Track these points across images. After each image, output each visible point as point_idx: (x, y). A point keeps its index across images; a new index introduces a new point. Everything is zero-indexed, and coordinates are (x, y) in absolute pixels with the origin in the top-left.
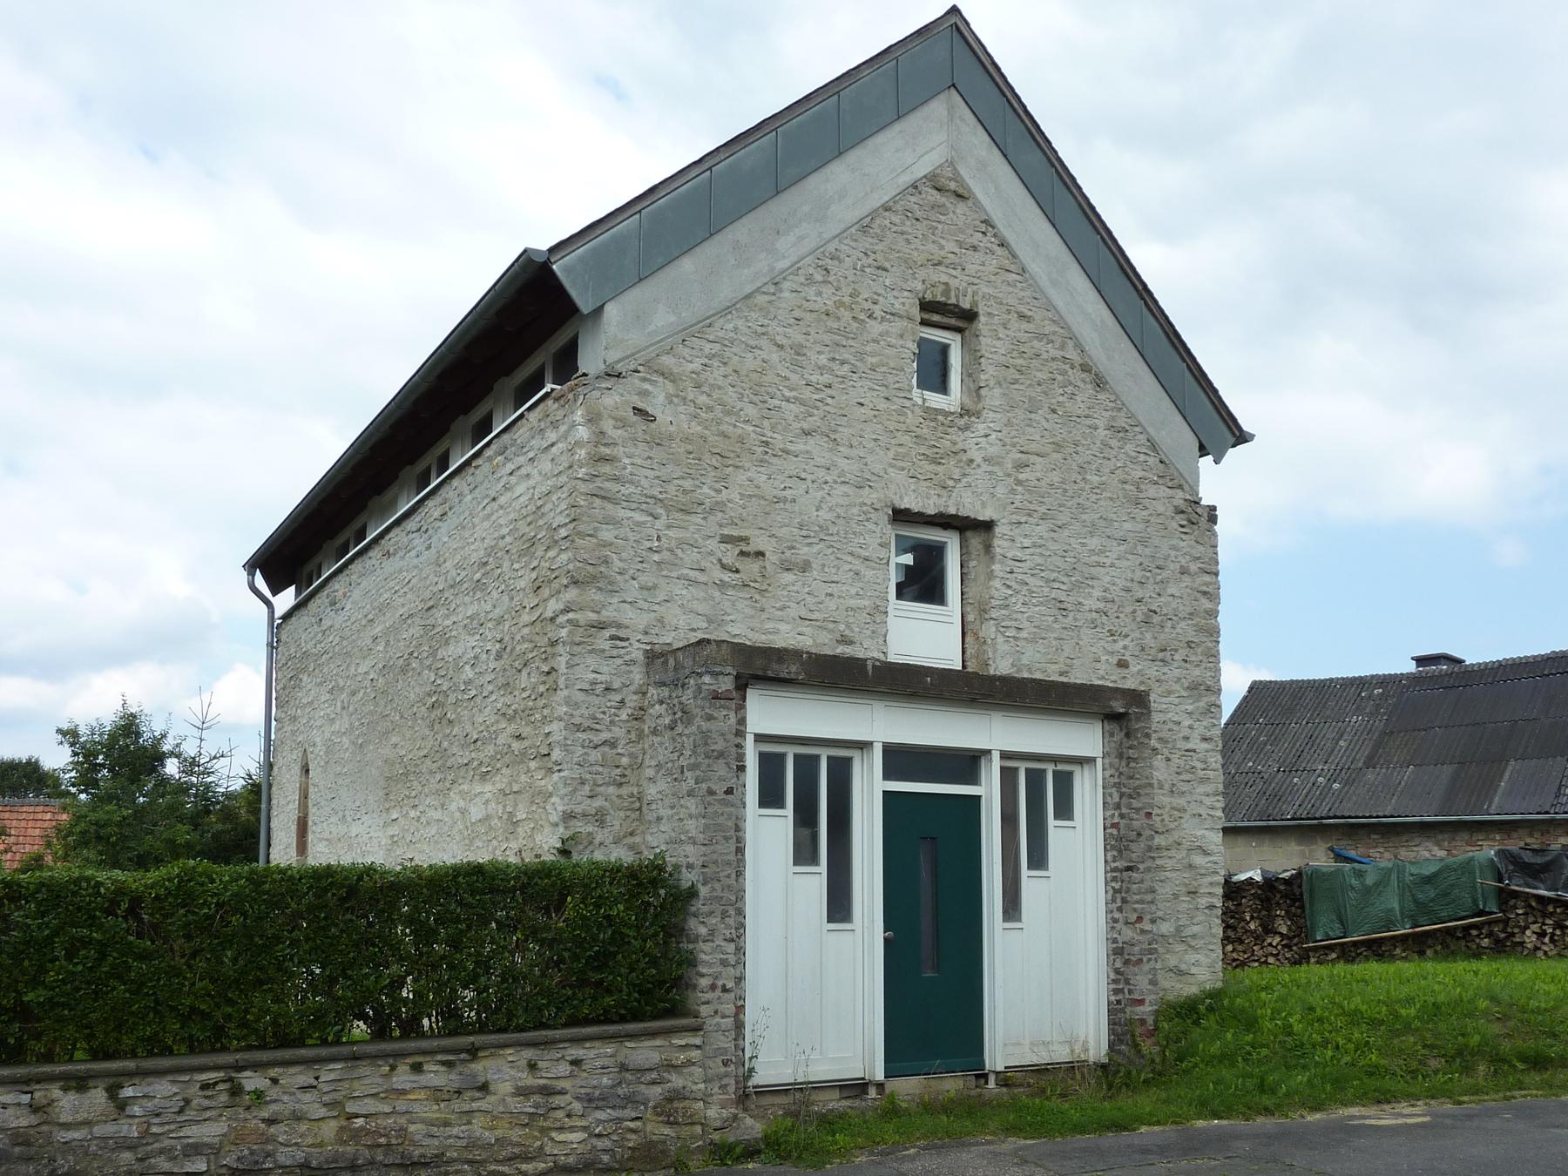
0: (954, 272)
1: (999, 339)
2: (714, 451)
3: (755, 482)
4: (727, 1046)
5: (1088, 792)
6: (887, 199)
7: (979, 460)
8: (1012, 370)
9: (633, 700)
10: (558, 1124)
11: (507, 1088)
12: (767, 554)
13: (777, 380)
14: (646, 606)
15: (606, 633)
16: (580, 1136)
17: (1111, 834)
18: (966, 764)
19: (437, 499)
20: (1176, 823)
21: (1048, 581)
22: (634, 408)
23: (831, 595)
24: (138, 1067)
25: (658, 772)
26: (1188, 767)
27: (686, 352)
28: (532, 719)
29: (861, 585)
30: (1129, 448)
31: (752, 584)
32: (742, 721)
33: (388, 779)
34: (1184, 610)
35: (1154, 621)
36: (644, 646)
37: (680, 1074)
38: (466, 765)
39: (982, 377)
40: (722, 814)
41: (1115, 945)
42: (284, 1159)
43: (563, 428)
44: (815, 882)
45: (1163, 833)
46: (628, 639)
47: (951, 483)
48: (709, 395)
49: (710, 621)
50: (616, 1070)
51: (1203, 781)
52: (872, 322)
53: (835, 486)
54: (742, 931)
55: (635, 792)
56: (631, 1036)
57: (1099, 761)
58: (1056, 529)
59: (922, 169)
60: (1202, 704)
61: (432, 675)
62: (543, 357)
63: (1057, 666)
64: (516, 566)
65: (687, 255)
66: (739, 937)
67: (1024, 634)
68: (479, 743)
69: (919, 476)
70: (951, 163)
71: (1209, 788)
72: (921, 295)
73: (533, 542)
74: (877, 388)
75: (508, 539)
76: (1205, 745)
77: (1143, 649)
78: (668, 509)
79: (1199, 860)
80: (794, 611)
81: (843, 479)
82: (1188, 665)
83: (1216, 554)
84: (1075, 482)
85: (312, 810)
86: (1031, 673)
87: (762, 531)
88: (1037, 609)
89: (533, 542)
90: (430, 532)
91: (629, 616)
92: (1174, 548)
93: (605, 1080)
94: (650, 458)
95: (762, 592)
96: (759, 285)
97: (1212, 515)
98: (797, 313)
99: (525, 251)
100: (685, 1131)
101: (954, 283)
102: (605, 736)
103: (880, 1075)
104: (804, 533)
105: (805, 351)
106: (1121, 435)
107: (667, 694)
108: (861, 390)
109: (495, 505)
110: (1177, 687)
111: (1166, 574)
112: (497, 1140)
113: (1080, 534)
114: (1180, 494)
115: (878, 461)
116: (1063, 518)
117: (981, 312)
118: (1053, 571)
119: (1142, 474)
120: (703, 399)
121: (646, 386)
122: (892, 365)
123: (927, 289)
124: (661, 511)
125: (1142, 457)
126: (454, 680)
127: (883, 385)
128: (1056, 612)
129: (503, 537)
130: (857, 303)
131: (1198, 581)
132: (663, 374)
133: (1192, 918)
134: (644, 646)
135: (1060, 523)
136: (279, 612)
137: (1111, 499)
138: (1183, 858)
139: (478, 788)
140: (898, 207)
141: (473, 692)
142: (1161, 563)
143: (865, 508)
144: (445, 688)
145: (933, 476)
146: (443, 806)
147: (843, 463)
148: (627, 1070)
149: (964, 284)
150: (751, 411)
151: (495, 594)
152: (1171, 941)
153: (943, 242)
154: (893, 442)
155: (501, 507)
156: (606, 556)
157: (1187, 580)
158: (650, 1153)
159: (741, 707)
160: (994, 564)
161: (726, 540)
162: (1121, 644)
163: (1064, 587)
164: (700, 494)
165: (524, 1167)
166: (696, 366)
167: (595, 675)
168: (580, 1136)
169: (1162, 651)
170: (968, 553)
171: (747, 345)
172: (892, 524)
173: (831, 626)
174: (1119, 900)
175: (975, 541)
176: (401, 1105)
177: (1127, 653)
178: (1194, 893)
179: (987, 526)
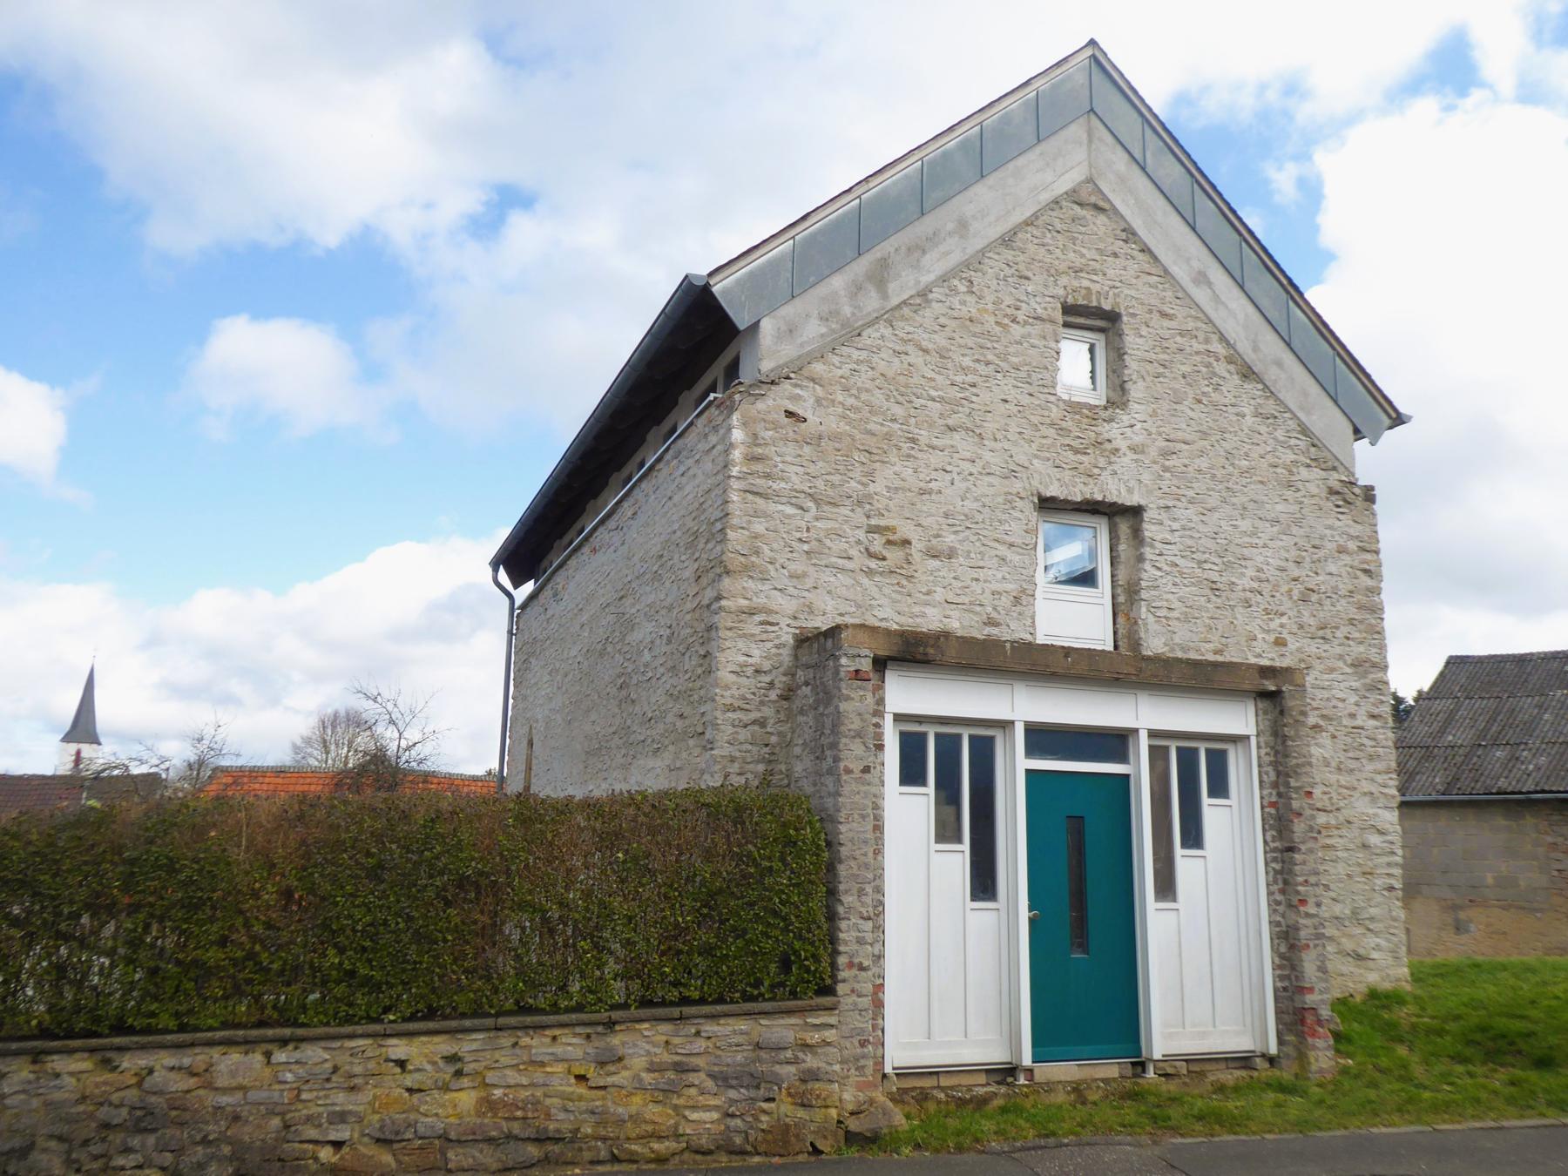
0: (1095, 278)
1: (1141, 336)
2: (861, 448)
3: (902, 476)
4: (865, 1025)
5: (1243, 772)
6: (1028, 214)
7: (1124, 449)
8: (1156, 365)
9: (781, 681)
10: (691, 1103)
11: (639, 1063)
12: (914, 542)
13: (923, 382)
14: (795, 592)
15: (758, 618)
16: (715, 1115)
17: (1269, 813)
18: (1114, 742)
19: (631, 500)
20: (1345, 801)
21: (1200, 563)
22: (786, 411)
23: (977, 580)
24: (292, 1033)
25: (803, 751)
27: (836, 360)
28: (692, 699)
30: (1280, 434)
31: (898, 570)
32: (881, 702)
33: (587, 753)
34: (1343, 589)
35: (1313, 599)
36: (793, 630)
37: (815, 1054)
38: (643, 741)
39: (1126, 372)
40: (858, 793)
41: (1278, 929)
42: (423, 1129)
43: (722, 431)
44: (957, 861)
45: (1331, 811)
46: (778, 624)
47: (1096, 471)
48: (856, 397)
49: (859, 606)
50: (749, 1048)
52: (1014, 326)
53: (980, 477)
54: (881, 909)
55: (783, 770)
56: (765, 1013)
57: (1253, 741)
58: (1206, 512)
59: (1064, 185)
61: (622, 658)
62: (717, 370)
63: (1211, 645)
64: (683, 558)
65: (837, 274)
66: (877, 915)
67: (1175, 614)
68: (652, 721)
69: (1064, 466)
70: (1090, 180)
71: (1380, 766)
72: (1062, 300)
73: (696, 535)
74: (1021, 385)
75: (679, 533)
76: (1373, 723)
78: (817, 502)
79: (1374, 839)
80: (940, 595)
81: (988, 471)
82: (1351, 643)
83: (1376, 532)
84: (1224, 467)
85: (533, 780)
86: (1185, 653)
87: (909, 521)
88: (1187, 589)
89: (696, 535)
90: (625, 529)
91: (781, 603)
92: (1330, 527)
93: (739, 1057)
94: (800, 456)
95: (909, 578)
96: (906, 297)
97: (1369, 495)
98: (942, 320)
99: (686, 276)
100: (819, 1115)
101: (1095, 287)
102: (755, 715)
103: (1027, 1061)
104: (950, 522)
105: (951, 354)
106: (1271, 421)
107: (811, 676)
108: (1006, 388)
109: (670, 504)
110: (1340, 664)
111: (1321, 553)
112: (631, 1116)
113: (1232, 516)
114: (1335, 475)
115: (1021, 454)
116: (1213, 501)
117: (1123, 313)
118: (1204, 553)
119: (1293, 457)
120: (851, 401)
121: (798, 391)
122: (1034, 364)
123: (1068, 294)
124: (811, 504)
125: (1293, 442)
126: (637, 663)
127: (1028, 383)
128: (1208, 592)
129: (675, 532)
130: (1000, 309)
132: (813, 380)
133: (1369, 900)
134: (793, 630)
135: (1209, 506)
136: (518, 603)
137: (1262, 482)
138: (1355, 837)
139: (651, 763)
140: (1039, 222)
141: (650, 674)
142: (1317, 542)
143: (1009, 497)
144: (629, 671)
145: (1077, 465)
146: (625, 779)
147: (988, 456)
148: (761, 1048)
149: (1107, 288)
150: (899, 411)
151: (668, 584)
152: (1347, 923)
153: (1084, 251)
154: (1037, 434)
155: (675, 505)
156: (758, 547)
157: (1347, 559)
158: (782, 1139)
159: (880, 687)
160: (1143, 546)
161: (872, 530)
162: (1277, 621)
163: (1216, 568)
164: (847, 488)
165: (656, 1146)
166: (845, 370)
167: (745, 658)
168: (715, 1115)
169: (1322, 628)
170: (1118, 538)
171: (894, 351)
172: (1039, 512)
173: (978, 609)
174: (1280, 882)
175: (1124, 528)
176: (539, 1077)
177: (1285, 631)
178: (1370, 874)
179: (1136, 512)
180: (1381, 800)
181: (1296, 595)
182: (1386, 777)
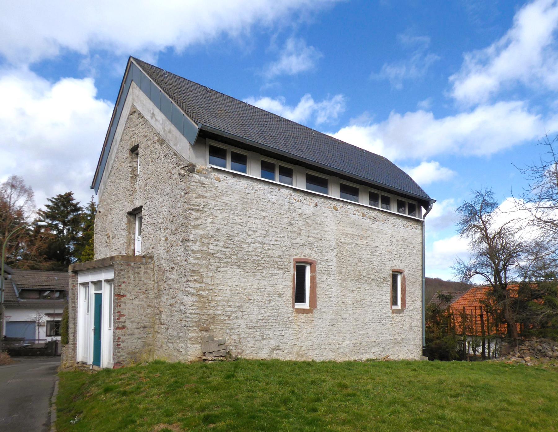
0: (134, 136)
163: (155, 218)
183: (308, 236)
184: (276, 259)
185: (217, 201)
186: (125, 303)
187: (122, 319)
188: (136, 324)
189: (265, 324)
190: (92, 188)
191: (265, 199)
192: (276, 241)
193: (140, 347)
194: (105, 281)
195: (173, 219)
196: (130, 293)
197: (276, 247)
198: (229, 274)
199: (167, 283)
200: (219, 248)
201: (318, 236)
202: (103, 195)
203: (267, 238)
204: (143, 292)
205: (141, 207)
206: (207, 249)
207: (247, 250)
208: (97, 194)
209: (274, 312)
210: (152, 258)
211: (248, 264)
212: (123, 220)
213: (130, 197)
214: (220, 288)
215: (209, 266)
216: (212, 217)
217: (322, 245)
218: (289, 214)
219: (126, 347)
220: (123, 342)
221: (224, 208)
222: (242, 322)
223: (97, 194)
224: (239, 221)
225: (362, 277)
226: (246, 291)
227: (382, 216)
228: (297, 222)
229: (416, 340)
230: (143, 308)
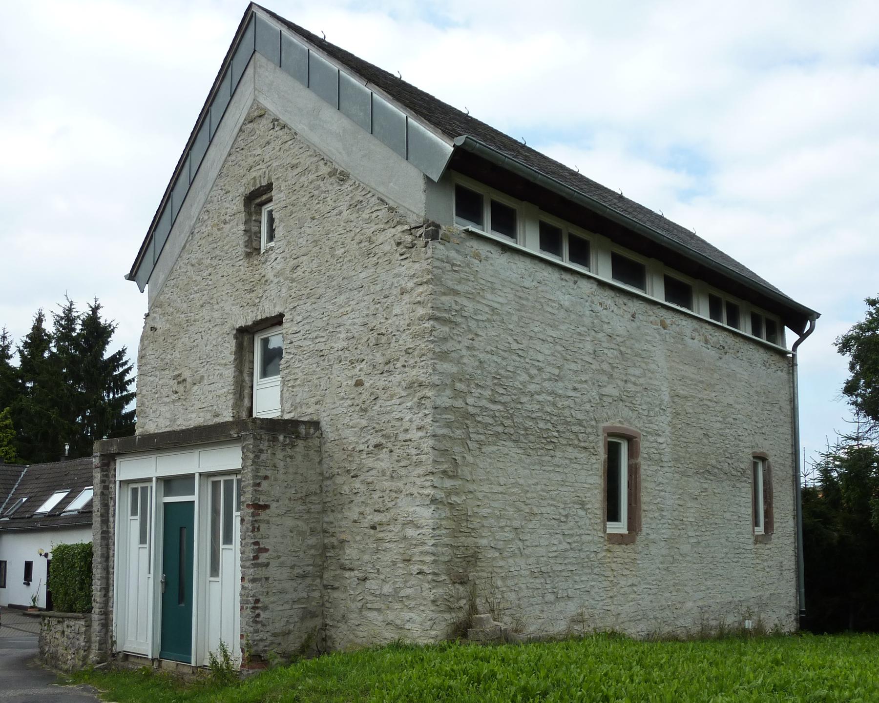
0: (258, 167)
20: (393, 503)
21: (313, 339)
26: (405, 454)
29: (223, 380)
45: (384, 511)
51: (419, 464)
60: (416, 399)
67: (298, 382)
76: (421, 434)
77: (374, 367)
79: (410, 532)
111: (390, 300)
128: (318, 359)
131: (415, 294)
163: (323, 340)
169: (387, 364)
173: (210, 408)
178: (409, 560)
180: (418, 499)
181: (373, 341)
182: (423, 479)
183: (626, 381)
184: (576, 428)
185: (478, 302)
186: (268, 522)
187: (263, 558)
188: (289, 570)
189: (560, 568)
190: (132, 277)
191: (554, 301)
192: (575, 389)
193: (296, 620)
194: (200, 474)
195: (377, 339)
196: (278, 501)
197: (575, 403)
198: (501, 459)
199: (361, 478)
200: (484, 403)
201: (641, 381)
202: (161, 292)
203: (560, 384)
204: (301, 498)
205: (281, 316)
206: (463, 405)
207: (529, 407)
208: (142, 291)
209: (575, 542)
210: (316, 424)
211: (532, 438)
212: (226, 345)
213: (248, 296)
214: (486, 488)
215: (469, 442)
216: (470, 337)
217: (649, 400)
218: (593, 333)
219: (271, 621)
220: (265, 608)
221: (489, 317)
222: (521, 562)
223: (142, 291)
224: (515, 346)
225: (709, 468)
226: (529, 495)
227: (733, 343)
228: (606, 351)
229: (789, 598)
230: (301, 533)
